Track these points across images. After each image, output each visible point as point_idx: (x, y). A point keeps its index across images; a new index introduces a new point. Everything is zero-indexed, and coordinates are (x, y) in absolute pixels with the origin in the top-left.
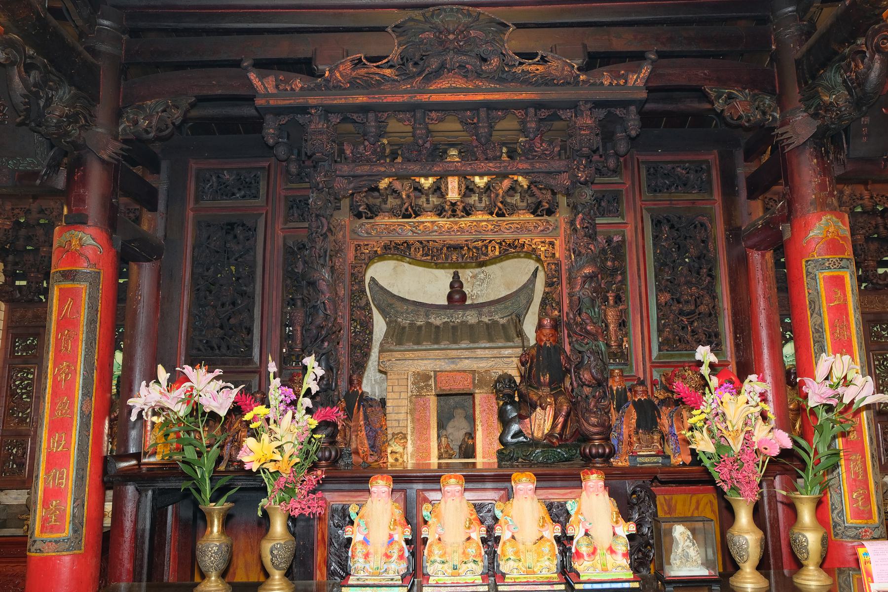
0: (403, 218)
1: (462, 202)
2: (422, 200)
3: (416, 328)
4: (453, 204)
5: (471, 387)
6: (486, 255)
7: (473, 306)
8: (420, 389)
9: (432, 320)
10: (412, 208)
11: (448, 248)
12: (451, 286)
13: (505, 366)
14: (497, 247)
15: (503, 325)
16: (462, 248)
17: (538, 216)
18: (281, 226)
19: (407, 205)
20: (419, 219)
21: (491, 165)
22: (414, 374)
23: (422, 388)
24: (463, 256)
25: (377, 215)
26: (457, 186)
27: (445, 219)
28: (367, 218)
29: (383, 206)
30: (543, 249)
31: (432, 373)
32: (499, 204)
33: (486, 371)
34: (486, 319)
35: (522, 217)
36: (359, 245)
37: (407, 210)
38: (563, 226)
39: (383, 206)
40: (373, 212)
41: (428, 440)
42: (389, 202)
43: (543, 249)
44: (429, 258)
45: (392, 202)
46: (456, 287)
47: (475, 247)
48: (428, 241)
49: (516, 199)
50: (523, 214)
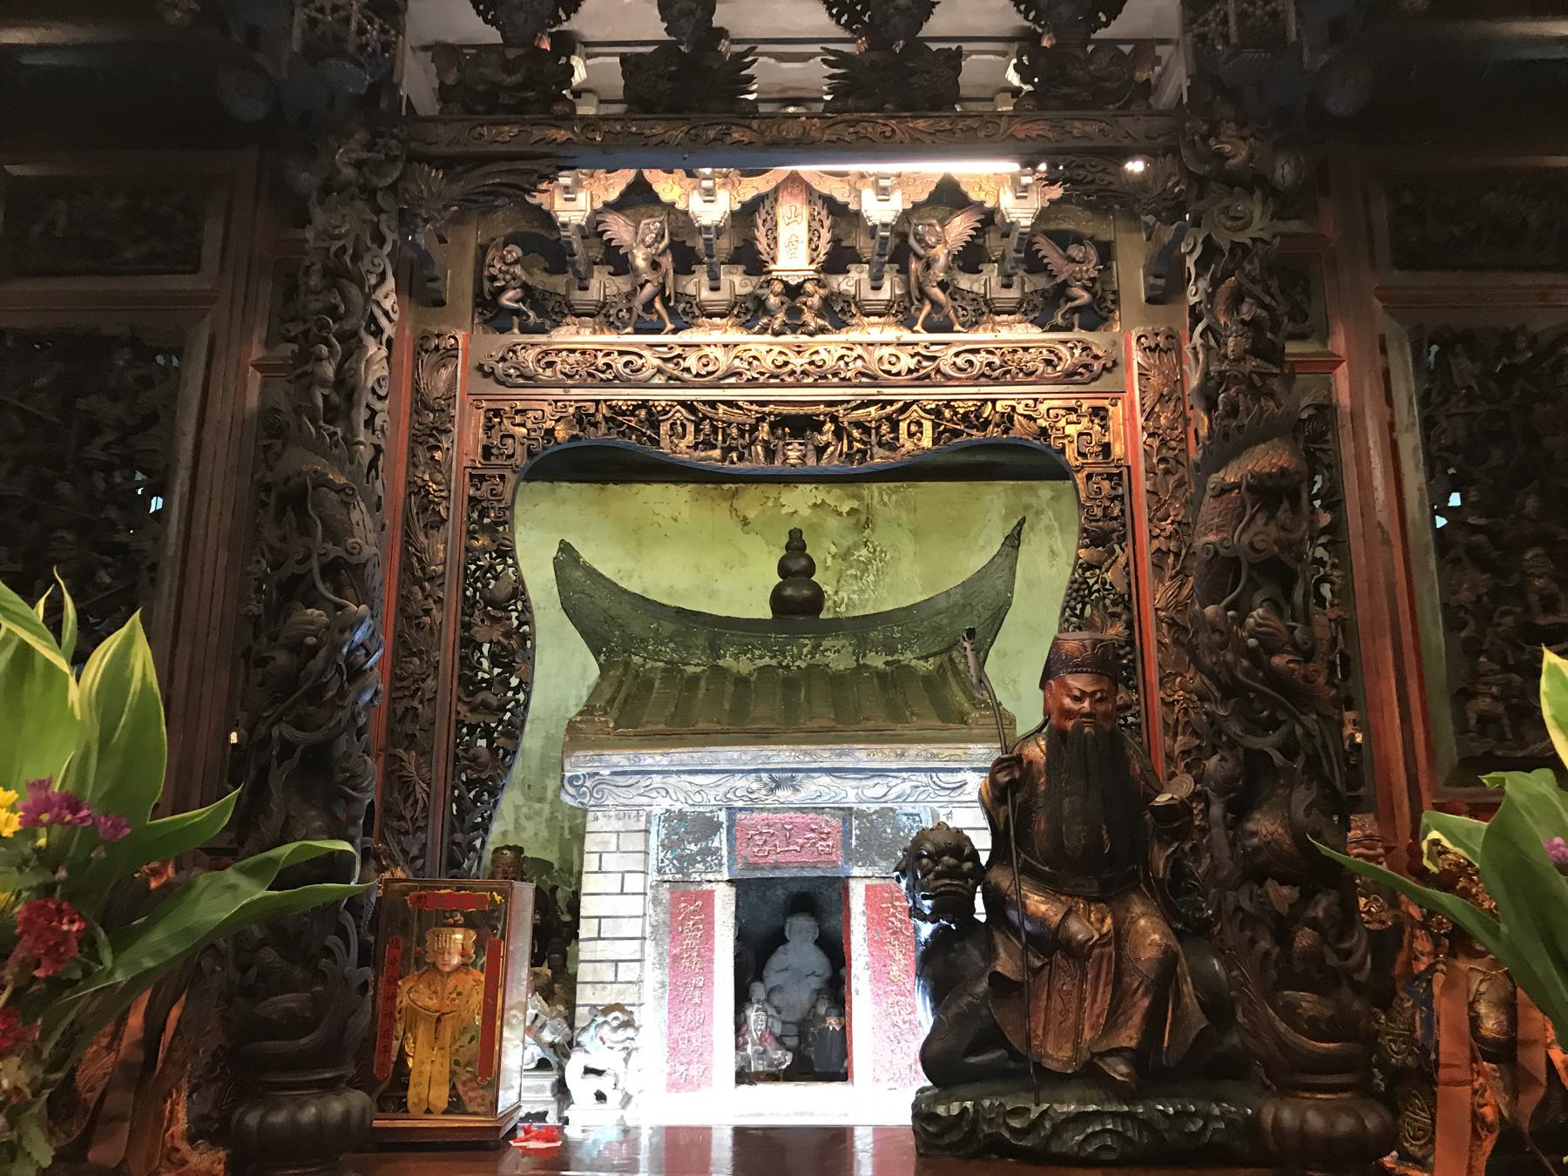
0: (637, 331)
1: (819, 283)
2: (697, 286)
3: (671, 679)
4: (793, 291)
5: (838, 856)
6: (892, 447)
7: (838, 626)
8: (684, 862)
9: (727, 662)
10: (665, 301)
11: (773, 426)
12: (783, 570)
13: (944, 796)
14: (927, 425)
15: (927, 679)
16: (818, 427)
17: (1055, 328)
18: (257, 352)
19: (649, 289)
20: (685, 337)
21: (921, 124)
22: (669, 816)
23: (692, 860)
24: (820, 451)
25: (558, 324)
26: (804, 235)
27: (768, 337)
28: (525, 330)
29: (577, 295)
30: (1072, 430)
31: (723, 816)
32: (937, 293)
33: (882, 813)
34: (877, 661)
35: (1005, 334)
36: (497, 413)
37: (649, 306)
38: (1137, 357)
39: (577, 295)
40: (549, 310)
41: (706, 1004)
42: (594, 283)
43: (1072, 430)
44: (717, 453)
45: (603, 284)
46: (796, 564)
47: (858, 424)
48: (713, 404)
49: (985, 282)
50: (1009, 324)
